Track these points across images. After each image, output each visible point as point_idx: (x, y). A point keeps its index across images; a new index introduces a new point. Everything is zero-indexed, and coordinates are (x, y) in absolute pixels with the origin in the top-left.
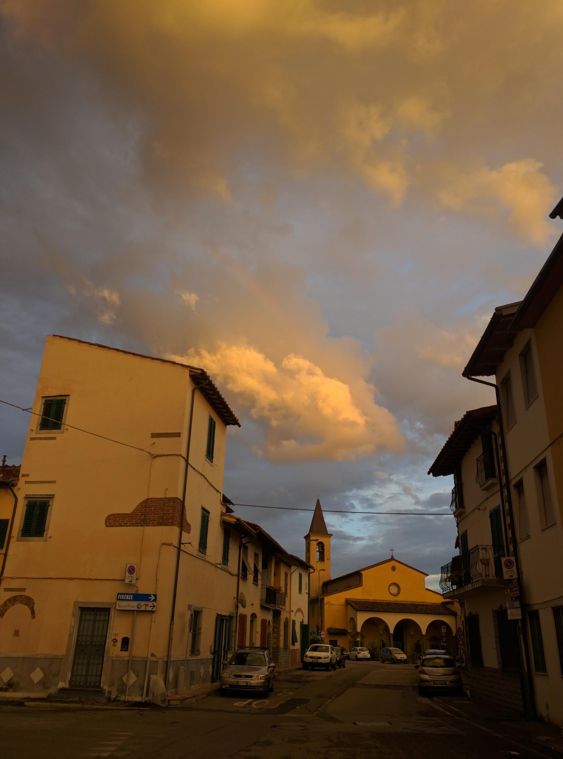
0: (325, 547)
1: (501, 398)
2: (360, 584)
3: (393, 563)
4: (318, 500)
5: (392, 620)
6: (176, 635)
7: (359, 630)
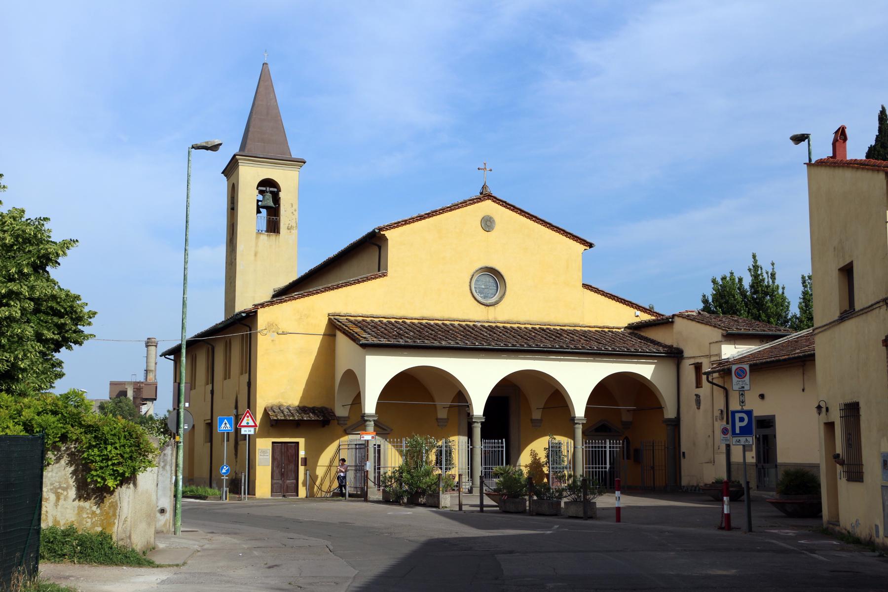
0: (281, 195)
1: (275, 474)
2: (380, 270)
3: (488, 207)
5: (479, 378)
7: (370, 406)
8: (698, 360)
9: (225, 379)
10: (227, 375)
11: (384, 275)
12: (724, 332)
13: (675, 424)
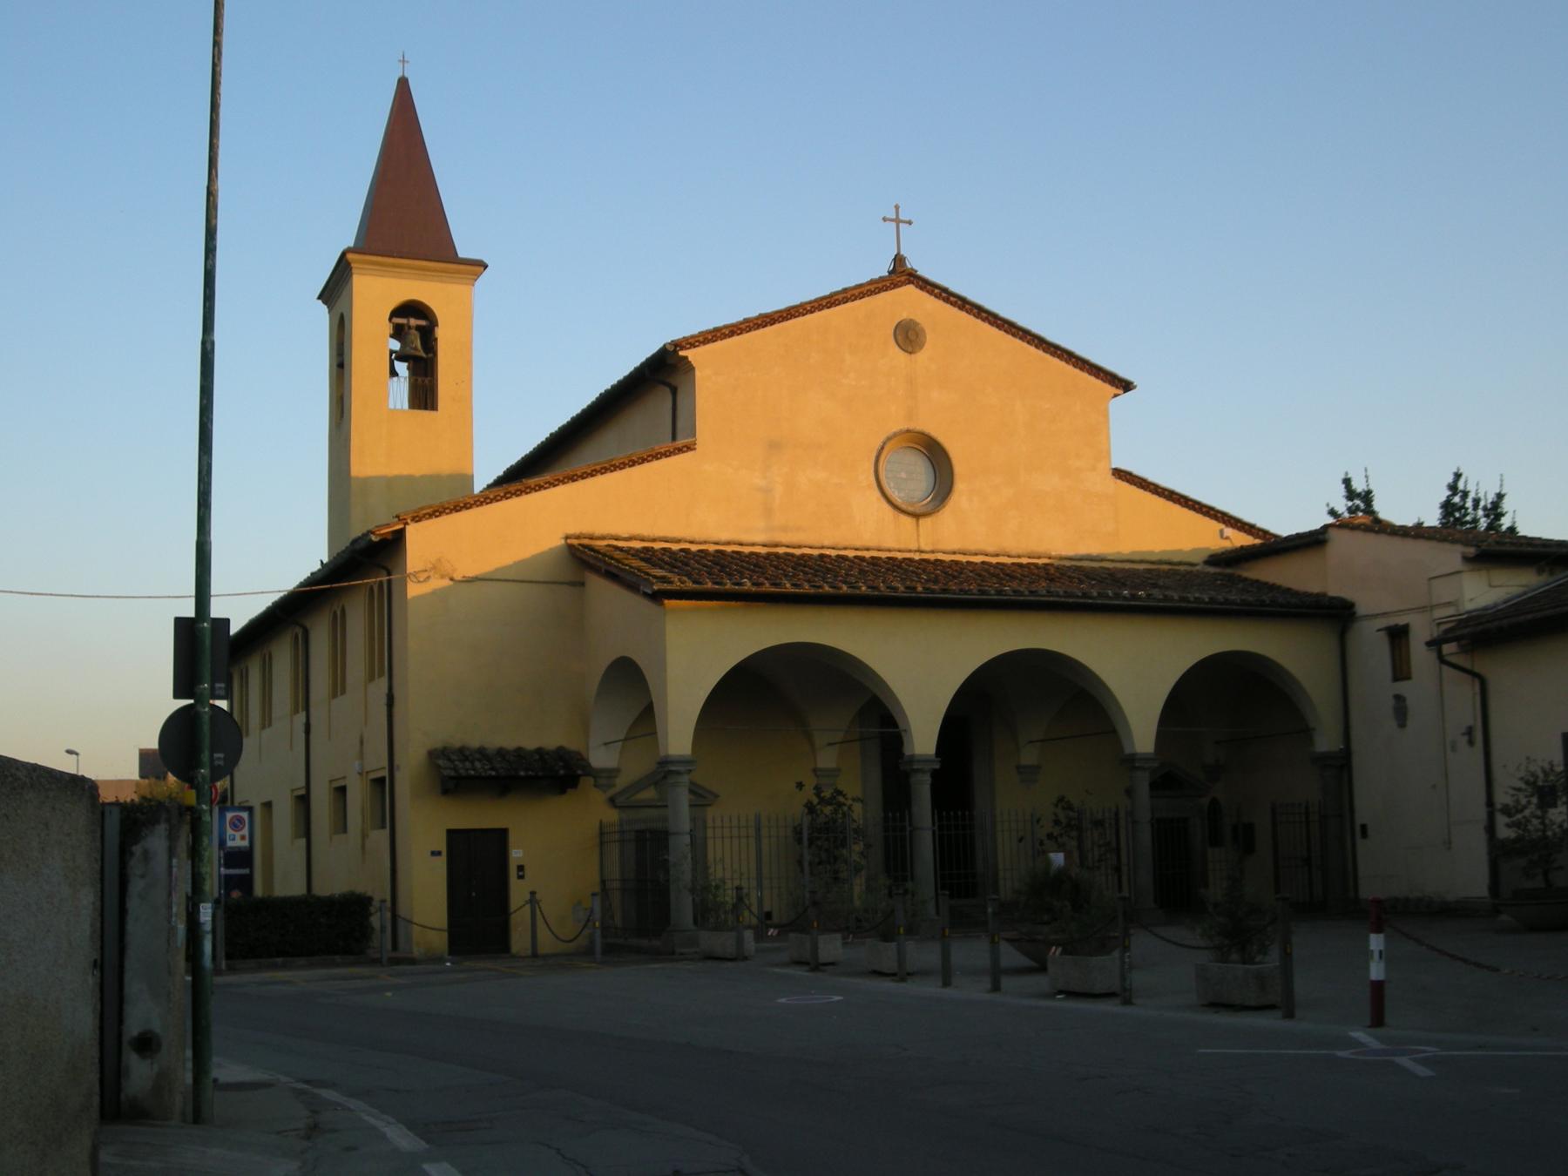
2: (678, 438)
3: (908, 302)
4: (403, 84)
6: (1468, 666)
7: (678, 736)
8: (1401, 621)
9: (334, 695)
10: (338, 687)
11: (690, 448)
12: (1471, 551)
13: (1341, 764)
